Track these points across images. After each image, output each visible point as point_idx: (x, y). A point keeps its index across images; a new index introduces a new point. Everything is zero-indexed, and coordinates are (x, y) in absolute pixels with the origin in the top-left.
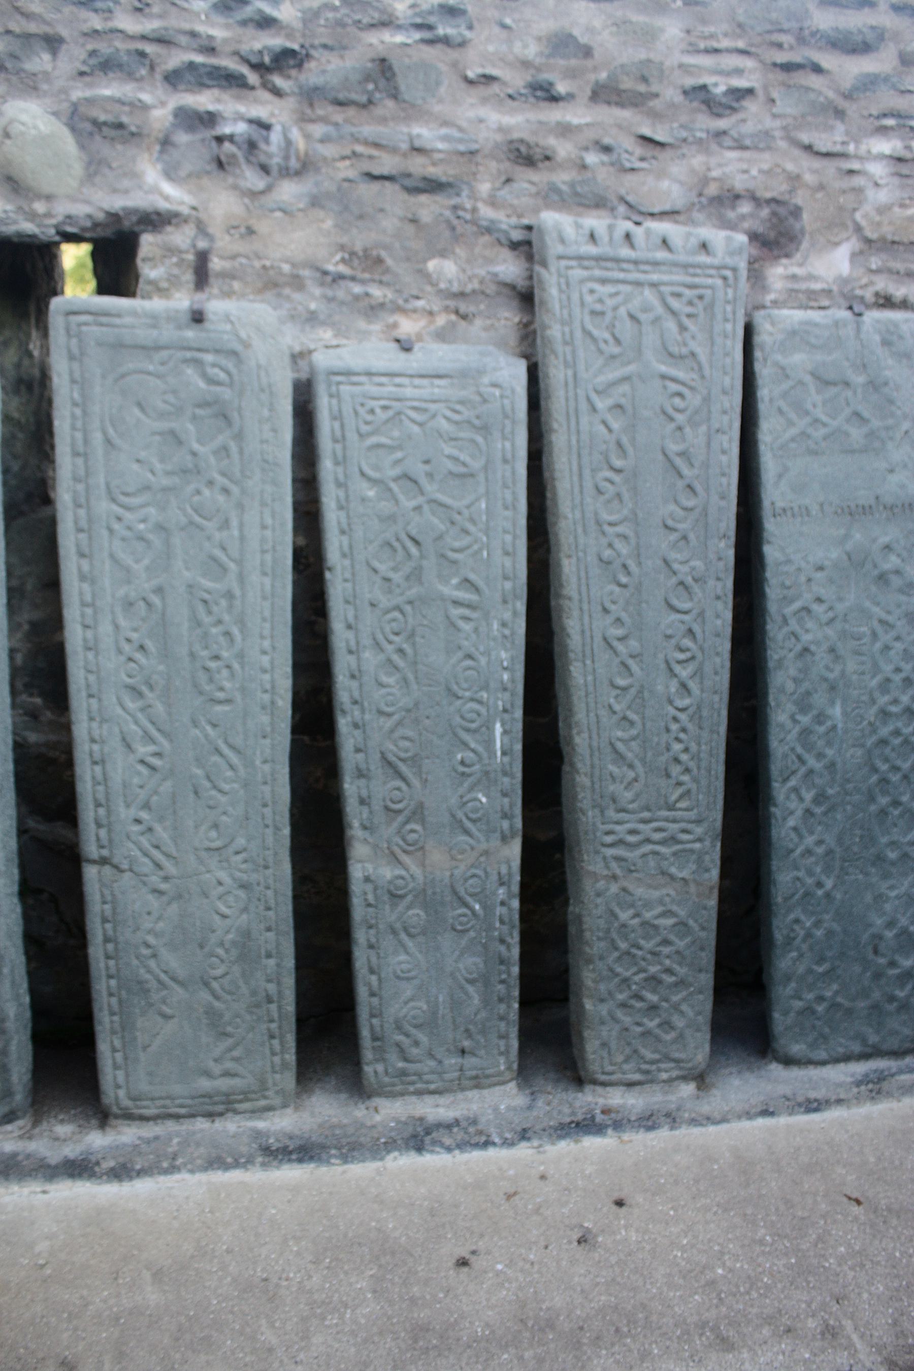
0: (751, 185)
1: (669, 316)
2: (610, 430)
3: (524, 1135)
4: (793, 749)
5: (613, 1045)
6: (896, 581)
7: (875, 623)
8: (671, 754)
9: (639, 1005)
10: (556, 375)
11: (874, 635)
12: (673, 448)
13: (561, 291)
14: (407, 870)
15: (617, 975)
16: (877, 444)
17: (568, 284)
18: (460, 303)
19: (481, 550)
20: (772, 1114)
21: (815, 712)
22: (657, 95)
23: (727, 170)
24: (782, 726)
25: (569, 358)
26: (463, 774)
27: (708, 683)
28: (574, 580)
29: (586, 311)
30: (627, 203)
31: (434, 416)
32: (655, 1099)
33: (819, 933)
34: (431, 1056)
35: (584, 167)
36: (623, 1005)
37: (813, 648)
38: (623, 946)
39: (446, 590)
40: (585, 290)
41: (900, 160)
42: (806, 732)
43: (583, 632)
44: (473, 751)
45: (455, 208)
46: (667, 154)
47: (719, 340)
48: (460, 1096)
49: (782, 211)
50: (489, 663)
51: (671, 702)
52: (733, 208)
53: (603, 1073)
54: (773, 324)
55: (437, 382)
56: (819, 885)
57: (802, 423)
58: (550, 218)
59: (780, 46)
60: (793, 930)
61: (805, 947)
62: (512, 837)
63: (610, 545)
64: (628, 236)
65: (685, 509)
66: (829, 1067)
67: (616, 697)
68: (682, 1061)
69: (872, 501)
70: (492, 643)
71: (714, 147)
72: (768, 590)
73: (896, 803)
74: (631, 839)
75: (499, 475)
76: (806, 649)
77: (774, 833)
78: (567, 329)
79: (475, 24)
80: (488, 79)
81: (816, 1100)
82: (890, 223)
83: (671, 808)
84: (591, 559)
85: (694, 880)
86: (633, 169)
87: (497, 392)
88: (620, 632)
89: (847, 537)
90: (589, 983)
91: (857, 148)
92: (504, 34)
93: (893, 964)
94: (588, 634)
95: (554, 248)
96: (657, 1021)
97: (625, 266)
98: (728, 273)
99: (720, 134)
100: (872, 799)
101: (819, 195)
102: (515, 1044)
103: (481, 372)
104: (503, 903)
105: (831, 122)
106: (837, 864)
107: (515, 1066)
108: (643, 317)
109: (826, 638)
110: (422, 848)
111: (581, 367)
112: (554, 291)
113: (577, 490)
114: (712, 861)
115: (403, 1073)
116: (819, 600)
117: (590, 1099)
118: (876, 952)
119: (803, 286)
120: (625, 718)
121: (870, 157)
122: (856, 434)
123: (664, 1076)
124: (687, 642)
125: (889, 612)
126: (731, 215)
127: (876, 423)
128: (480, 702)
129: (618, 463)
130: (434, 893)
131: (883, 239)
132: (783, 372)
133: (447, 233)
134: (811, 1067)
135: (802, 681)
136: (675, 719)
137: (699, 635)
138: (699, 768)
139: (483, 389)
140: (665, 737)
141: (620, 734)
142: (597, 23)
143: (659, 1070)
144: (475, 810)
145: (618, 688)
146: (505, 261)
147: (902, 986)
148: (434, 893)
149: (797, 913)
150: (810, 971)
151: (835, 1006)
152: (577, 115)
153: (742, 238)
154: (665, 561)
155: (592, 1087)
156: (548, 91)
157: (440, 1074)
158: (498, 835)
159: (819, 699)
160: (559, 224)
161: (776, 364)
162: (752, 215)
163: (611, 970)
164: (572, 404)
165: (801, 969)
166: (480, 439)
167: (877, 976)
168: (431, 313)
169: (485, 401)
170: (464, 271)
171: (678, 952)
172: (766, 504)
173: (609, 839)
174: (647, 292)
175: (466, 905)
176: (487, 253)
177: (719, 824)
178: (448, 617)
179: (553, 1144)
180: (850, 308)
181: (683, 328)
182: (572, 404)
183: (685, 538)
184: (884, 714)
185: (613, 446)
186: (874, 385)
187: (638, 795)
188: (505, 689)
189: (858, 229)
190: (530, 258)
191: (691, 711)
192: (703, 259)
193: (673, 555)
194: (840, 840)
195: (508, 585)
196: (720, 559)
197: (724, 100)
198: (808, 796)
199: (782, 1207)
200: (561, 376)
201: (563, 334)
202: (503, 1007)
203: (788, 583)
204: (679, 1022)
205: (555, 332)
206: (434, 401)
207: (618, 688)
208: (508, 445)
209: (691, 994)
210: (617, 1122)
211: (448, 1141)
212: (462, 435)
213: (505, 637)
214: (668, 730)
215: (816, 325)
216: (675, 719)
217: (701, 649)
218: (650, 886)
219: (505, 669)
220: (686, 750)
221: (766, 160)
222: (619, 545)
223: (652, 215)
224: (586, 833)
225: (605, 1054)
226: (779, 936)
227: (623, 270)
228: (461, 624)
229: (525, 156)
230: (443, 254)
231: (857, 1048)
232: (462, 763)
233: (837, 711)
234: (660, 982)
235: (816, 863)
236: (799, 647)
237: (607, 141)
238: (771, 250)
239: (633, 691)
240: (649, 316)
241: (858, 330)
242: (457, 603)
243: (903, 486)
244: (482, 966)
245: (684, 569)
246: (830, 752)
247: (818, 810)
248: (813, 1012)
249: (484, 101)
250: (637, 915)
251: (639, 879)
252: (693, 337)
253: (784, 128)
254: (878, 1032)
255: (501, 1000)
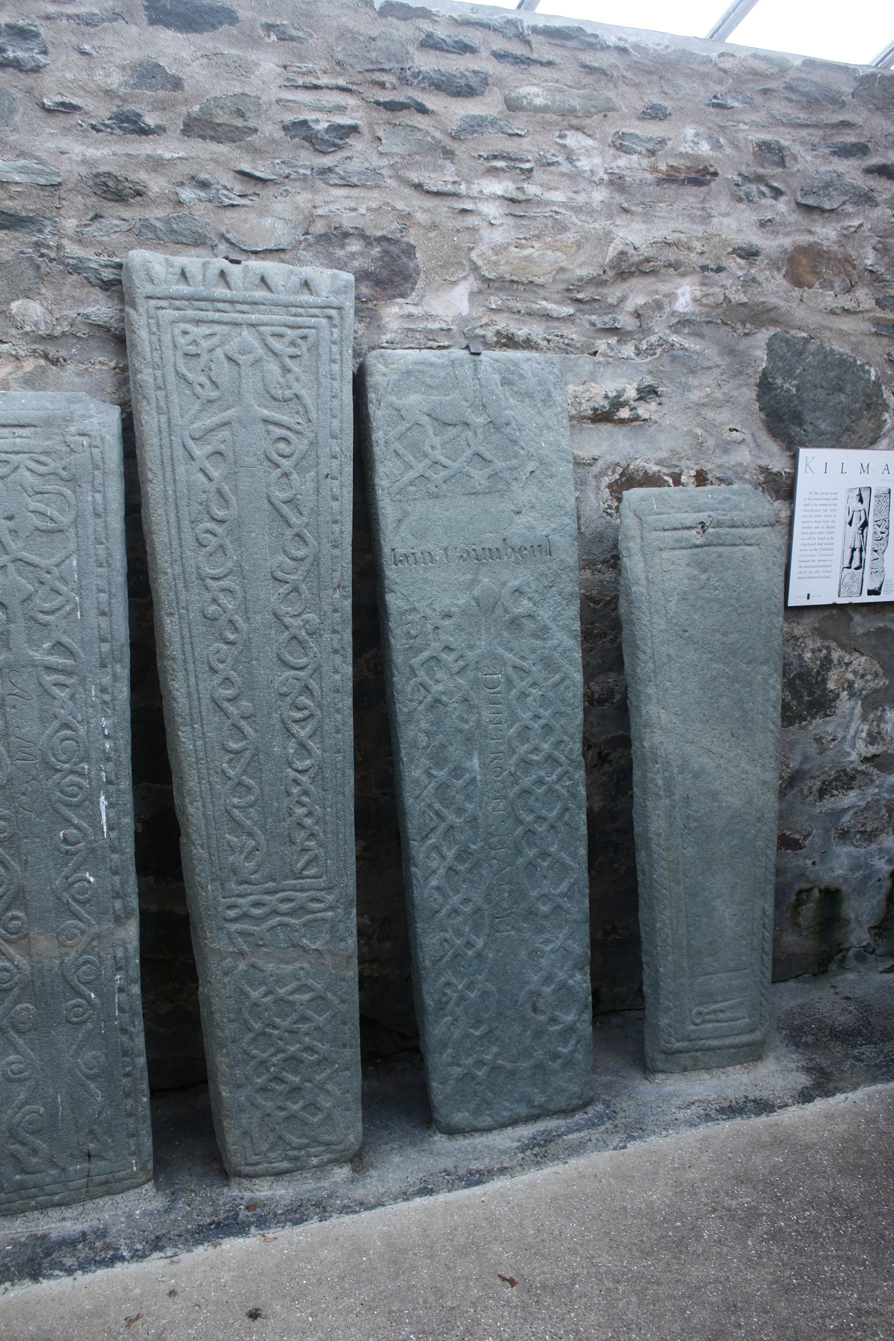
0: (360, 223)
1: (272, 358)
2: (210, 480)
3: (157, 1245)
4: (430, 806)
5: (255, 1133)
6: (529, 625)
7: (510, 670)
8: (293, 819)
9: (279, 1088)
10: (149, 422)
11: (509, 681)
12: (280, 495)
13: (152, 333)
14: (11, 961)
15: (254, 1057)
16: (501, 485)
17: (158, 325)
18: (49, 347)
19: (74, 610)
20: (430, 1192)
21: (451, 766)
22: (256, 131)
23: (333, 208)
24: (417, 781)
25: (162, 403)
26: (67, 852)
27: (329, 742)
28: (176, 639)
29: (179, 353)
30: (227, 240)
31: (17, 468)
32: (307, 1187)
33: (473, 995)
34: (54, 1164)
35: (180, 203)
36: (263, 1089)
37: (444, 698)
38: (257, 1026)
39: (37, 656)
40: (177, 331)
41: (513, 200)
42: (442, 787)
43: (189, 694)
44: (77, 827)
45: (38, 245)
46: (271, 190)
47: (326, 382)
48: (90, 1205)
49: (393, 249)
50: (88, 732)
51: (290, 765)
52: (343, 247)
53: (247, 1164)
54: (386, 365)
55: (19, 431)
56: (469, 945)
57: (421, 466)
58: (138, 256)
59: (382, 85)
60: (445, 994)
61: (458, 1011)
62: (127, 918)
63: (215, 601)
64: (222, 274)
65: (295, 559)
66: (495, 1132)
67: (229, 762)
68: (333, 1144)
69: (499, 544)
70: (91, 710)
71: (320, 184)
72: (392, 641)
73: (544, 855)
74: (256, 911)
75: (90, 530)
76: (437, 701)
77: (416, 893)
78: (159, 373)
79: (51, 49)
80: (69, 108)
81: (478, 1171)
82: (507, 263)
83: (299, 876)
84: (194, 615)
85: (329, 951)
86: (233, 206)
87: (85, 441)
88: (230, 692)
89: (474, 582)
90: (224, 1068)
91: (468, 188)
92: (83, 61)
93: (553, 1020)
94: (195, 696)
95: (142, 288)
96: (301, 1103)
97: (220, 305)
98: (333, 312)
99: (326, 171)
100: (519, 852)
101: (432, 234)
102: (148, 1142)
103: (68, 420)
104: (121, 990)
105: (440, 162)
106: (487, 921)
107: (150, 1166)
108: (241, 359)
109: (458, 687)
110: (26, 936)
111: (175, 412)
112: (143, 333)
113: (175, 543)
114: (347, 929)
115: (22, 1186)
116: (448, 649)
117: (237, 1193)
118: (535, 1009)
119: (420, 325)
120: (240, 783)
121: (481, 197)
122: (479, 475)
123: (315, 1161)
124: (304, 700)
125: (523, 658)
126: (340, 253)
127: (499, 464)
128: (81, 774)
129: (220, 514)
130: (43, 985)
131: (501, 279)
132: (399, 414)
133: (31, 273)
134: (477, 1135)
135: (435, 733)
136: (296, 782)
137: (317, 692)
138: (325, 832)
139: (69, 439)
140: (286, 802)
141: (236, 800)
142: (186, 54)
143: (309, 1156)
144: (83, 891)
145: (231, 752)
146: (97, 302)
147: (565, 1043)
148: (43, 985)
149: (448, 976)
150: (468, 1035)
151: (495, 1069)
152: (169, 148)
153: (348, 277)
154: (276, 615)
155: (237, 1179)
156: (136, 122)
157: (64, 1183)
158: (110, 916)
159: (455, 752)
160: (151, 263)
161: (390, 405)
162: (362, 254)
163: (246, 1053)
164: (167, 452)
165: (457, 1034)
166: (68, 492)
167: (539, 1034)
168: (17, 358)
169: (73, 451)
170: (51, 312)
171: (317, 1028)
172: (386, 550)
173: (232, 913)
174: (245, 332)
175: (82, 996)
176: (76, 293)
177: (352, 890)
178: (41, 685)
179: (189, 1251)
180: (467, 347)
181: (286, 370)
182: (167, 452)
183: (296, 589)
184: (525, 763)
185: (213, 495)
186: (495, 425)
187: (260, 865)
188: (108, 759)
189: (475, 268)
190: (121, 298)
191: (312, 772)
192: (306, 298)
193: (284, 609)
194: (487, 897)
195: (105, 647)
196: (335, 611)
197: (327, 137)
198: (450, 854)
199: (431, 1298)
200: (154, 423)
201: (155, 378)
202: (130, 1102)
203: (413, 632)
204: (326, 1103)
205: (146, 376)
206: (17, 453)
207: (231, 752)
208: (98, 496)
209: (336, 1071)
210: (262, 1218)
211: (69, 1262)
212: (49, 488)
213: (105, 703)
214: (289, 794)
215: (432, 365)
216: (296, 782)
217: (319, 705)
218: (282, 961)
219: (107, 737)
220: (310, 814)
221: (374, 199)
222: (224, 600)
223: (256, 253)
224: (207, 909)
225: (247, 1143)
226: (430, 1002)
227: (219, 311)
228: (56, 690)
229: (114, 191)
230: (27, 294)
231: (523, 1110)
232: (65, 840)
233: (475, 763)
234: (301, 1061)
235: (464, 923)
236: (429, 699)
237: (203, 176)
238: (385, 289)
239: (247, 754)
240: (250, 358)
241: (476, 370)
242: (49, 669)
243: (531, 528)
244: (102, 1059)
245: (298, 622)
246: (470, 806)
247: (462, 868)
248: (474, 1078)
249: (66, 131)
250: (269, 993)
251: (268, 954)
252: (297, 380)
253: (392, 166)
254: (543, 1092)
255: (127, 1095)
